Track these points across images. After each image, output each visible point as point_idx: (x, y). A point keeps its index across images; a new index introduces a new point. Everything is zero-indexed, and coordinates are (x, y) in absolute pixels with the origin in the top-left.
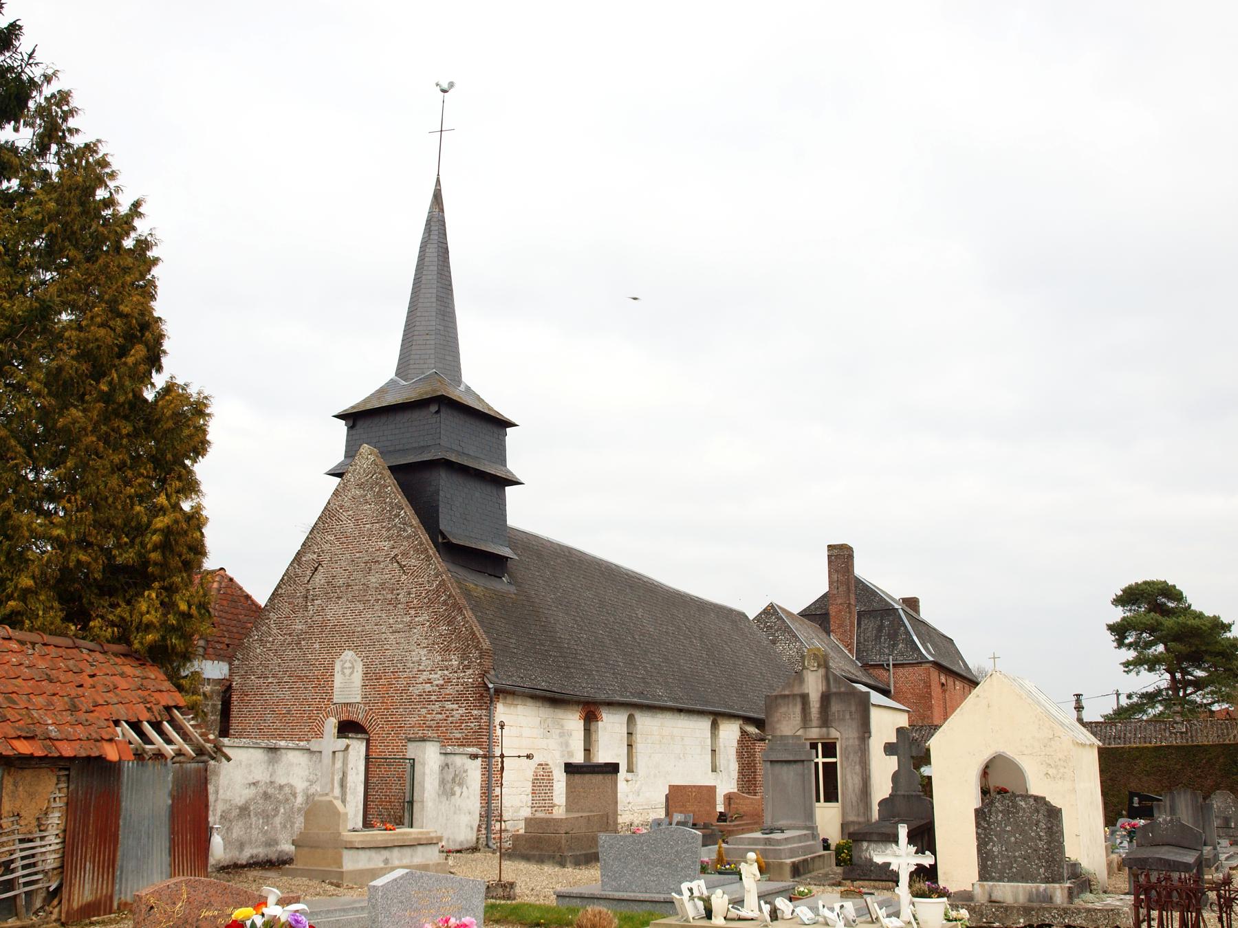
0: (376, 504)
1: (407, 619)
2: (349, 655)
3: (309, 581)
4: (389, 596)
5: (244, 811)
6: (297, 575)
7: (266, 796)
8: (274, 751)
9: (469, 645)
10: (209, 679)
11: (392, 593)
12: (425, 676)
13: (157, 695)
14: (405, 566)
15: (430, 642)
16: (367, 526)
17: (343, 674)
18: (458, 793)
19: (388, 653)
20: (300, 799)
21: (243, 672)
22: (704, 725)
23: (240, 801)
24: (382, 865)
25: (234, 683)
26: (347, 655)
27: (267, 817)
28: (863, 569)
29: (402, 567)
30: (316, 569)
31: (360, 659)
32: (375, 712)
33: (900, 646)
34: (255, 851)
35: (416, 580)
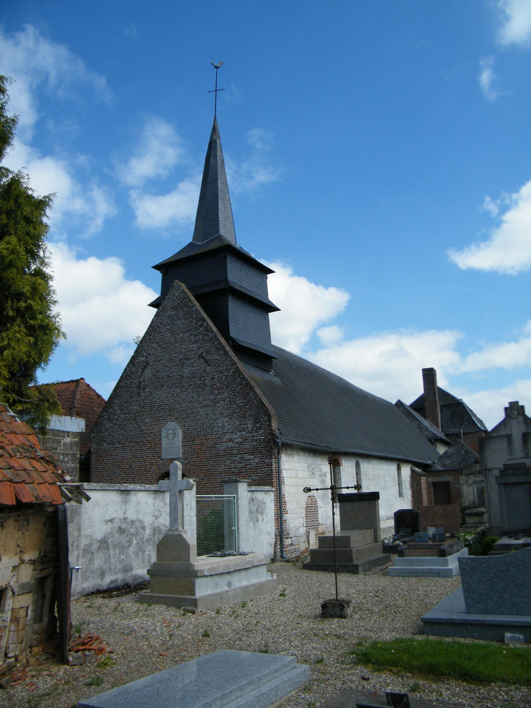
0: (186, 319)
1: (213, 397)
2: (172, 425)
3: (140, 376)
4: (198, 382)
5: (104, 543)
6: (132, 373)
7: (121, 530)
8: (125, 492)
9: (260, 412)
10: (68, 432)
11: (200, 380)
12: (228, 436)
13: (11, 437)
14: (208, 360)
15: (231, 412)
16: (180, 335)
17: (168, 438)
18: (261, 520)
19: (200, 422)
20: (148, 531)
21: (97, 441)
22: (392, 468)
23: (99, 536)
24: (226, 588)
25: (92, 449)
26: (170, 425)
27: (122, 548)
28: (441, 383)
29: (206, 361)
30: (145, 367)
31: (179, 427)
32: (192, 464)
33: (466, 423)
34: (113, 577)
35: (217, 369)
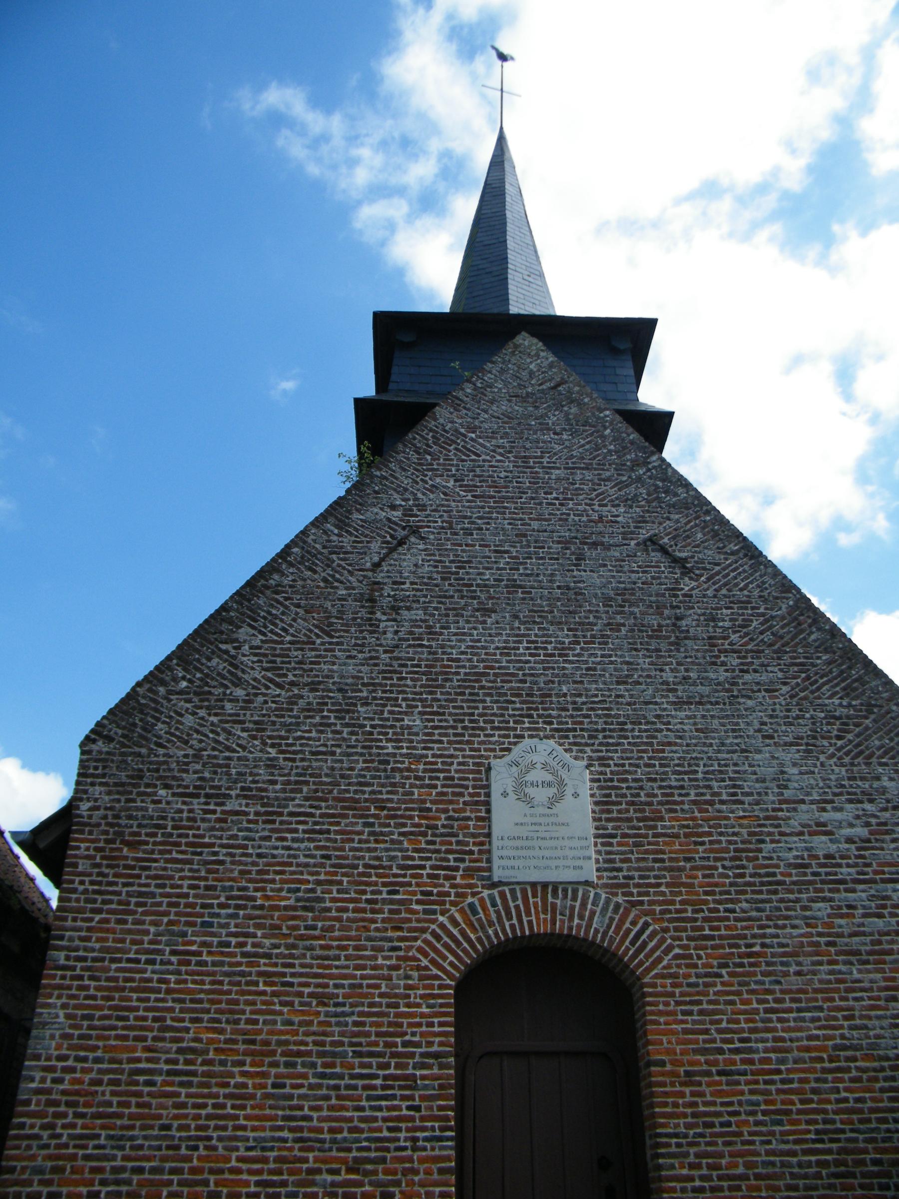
19: (674, 754)
32: (651, 913)
